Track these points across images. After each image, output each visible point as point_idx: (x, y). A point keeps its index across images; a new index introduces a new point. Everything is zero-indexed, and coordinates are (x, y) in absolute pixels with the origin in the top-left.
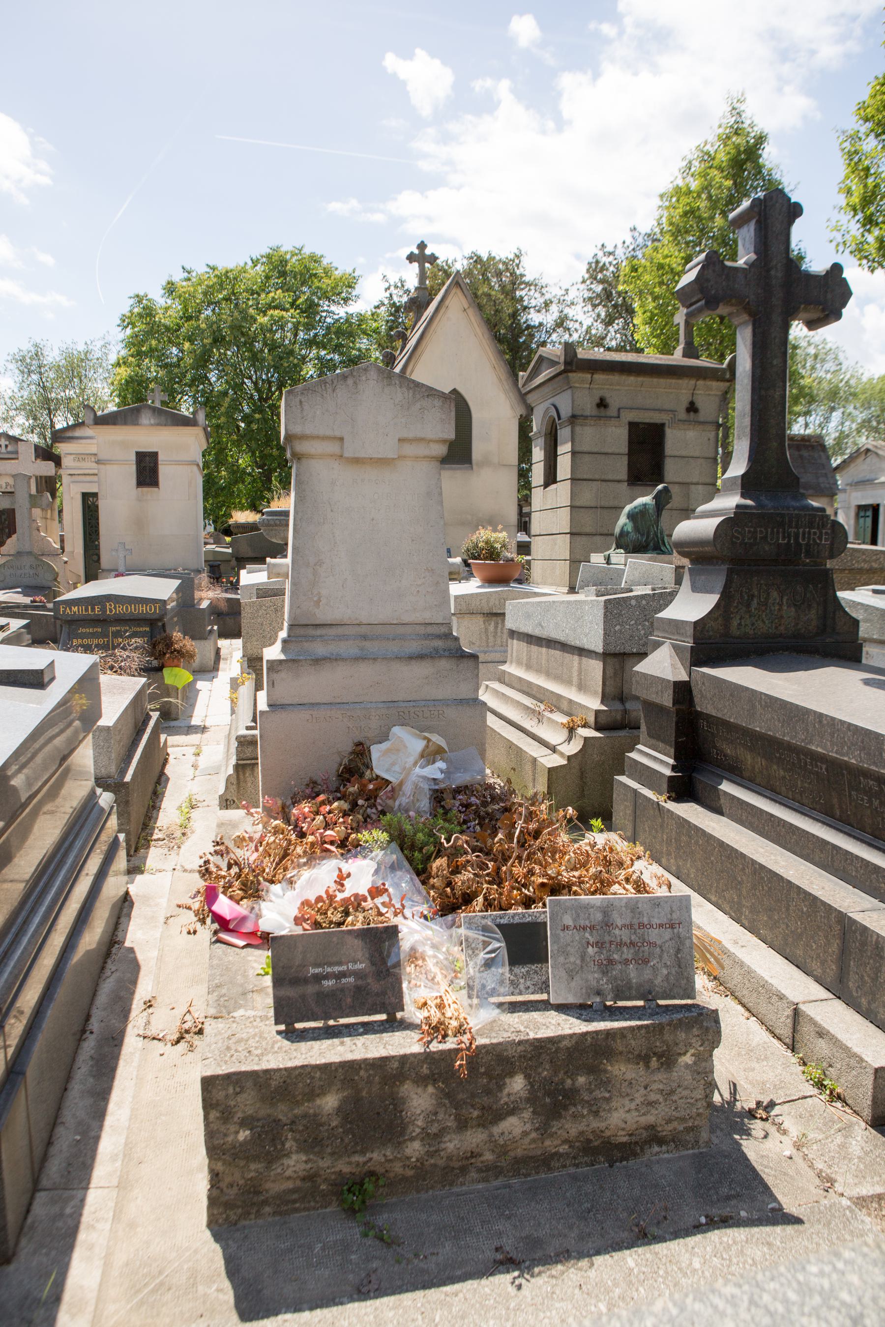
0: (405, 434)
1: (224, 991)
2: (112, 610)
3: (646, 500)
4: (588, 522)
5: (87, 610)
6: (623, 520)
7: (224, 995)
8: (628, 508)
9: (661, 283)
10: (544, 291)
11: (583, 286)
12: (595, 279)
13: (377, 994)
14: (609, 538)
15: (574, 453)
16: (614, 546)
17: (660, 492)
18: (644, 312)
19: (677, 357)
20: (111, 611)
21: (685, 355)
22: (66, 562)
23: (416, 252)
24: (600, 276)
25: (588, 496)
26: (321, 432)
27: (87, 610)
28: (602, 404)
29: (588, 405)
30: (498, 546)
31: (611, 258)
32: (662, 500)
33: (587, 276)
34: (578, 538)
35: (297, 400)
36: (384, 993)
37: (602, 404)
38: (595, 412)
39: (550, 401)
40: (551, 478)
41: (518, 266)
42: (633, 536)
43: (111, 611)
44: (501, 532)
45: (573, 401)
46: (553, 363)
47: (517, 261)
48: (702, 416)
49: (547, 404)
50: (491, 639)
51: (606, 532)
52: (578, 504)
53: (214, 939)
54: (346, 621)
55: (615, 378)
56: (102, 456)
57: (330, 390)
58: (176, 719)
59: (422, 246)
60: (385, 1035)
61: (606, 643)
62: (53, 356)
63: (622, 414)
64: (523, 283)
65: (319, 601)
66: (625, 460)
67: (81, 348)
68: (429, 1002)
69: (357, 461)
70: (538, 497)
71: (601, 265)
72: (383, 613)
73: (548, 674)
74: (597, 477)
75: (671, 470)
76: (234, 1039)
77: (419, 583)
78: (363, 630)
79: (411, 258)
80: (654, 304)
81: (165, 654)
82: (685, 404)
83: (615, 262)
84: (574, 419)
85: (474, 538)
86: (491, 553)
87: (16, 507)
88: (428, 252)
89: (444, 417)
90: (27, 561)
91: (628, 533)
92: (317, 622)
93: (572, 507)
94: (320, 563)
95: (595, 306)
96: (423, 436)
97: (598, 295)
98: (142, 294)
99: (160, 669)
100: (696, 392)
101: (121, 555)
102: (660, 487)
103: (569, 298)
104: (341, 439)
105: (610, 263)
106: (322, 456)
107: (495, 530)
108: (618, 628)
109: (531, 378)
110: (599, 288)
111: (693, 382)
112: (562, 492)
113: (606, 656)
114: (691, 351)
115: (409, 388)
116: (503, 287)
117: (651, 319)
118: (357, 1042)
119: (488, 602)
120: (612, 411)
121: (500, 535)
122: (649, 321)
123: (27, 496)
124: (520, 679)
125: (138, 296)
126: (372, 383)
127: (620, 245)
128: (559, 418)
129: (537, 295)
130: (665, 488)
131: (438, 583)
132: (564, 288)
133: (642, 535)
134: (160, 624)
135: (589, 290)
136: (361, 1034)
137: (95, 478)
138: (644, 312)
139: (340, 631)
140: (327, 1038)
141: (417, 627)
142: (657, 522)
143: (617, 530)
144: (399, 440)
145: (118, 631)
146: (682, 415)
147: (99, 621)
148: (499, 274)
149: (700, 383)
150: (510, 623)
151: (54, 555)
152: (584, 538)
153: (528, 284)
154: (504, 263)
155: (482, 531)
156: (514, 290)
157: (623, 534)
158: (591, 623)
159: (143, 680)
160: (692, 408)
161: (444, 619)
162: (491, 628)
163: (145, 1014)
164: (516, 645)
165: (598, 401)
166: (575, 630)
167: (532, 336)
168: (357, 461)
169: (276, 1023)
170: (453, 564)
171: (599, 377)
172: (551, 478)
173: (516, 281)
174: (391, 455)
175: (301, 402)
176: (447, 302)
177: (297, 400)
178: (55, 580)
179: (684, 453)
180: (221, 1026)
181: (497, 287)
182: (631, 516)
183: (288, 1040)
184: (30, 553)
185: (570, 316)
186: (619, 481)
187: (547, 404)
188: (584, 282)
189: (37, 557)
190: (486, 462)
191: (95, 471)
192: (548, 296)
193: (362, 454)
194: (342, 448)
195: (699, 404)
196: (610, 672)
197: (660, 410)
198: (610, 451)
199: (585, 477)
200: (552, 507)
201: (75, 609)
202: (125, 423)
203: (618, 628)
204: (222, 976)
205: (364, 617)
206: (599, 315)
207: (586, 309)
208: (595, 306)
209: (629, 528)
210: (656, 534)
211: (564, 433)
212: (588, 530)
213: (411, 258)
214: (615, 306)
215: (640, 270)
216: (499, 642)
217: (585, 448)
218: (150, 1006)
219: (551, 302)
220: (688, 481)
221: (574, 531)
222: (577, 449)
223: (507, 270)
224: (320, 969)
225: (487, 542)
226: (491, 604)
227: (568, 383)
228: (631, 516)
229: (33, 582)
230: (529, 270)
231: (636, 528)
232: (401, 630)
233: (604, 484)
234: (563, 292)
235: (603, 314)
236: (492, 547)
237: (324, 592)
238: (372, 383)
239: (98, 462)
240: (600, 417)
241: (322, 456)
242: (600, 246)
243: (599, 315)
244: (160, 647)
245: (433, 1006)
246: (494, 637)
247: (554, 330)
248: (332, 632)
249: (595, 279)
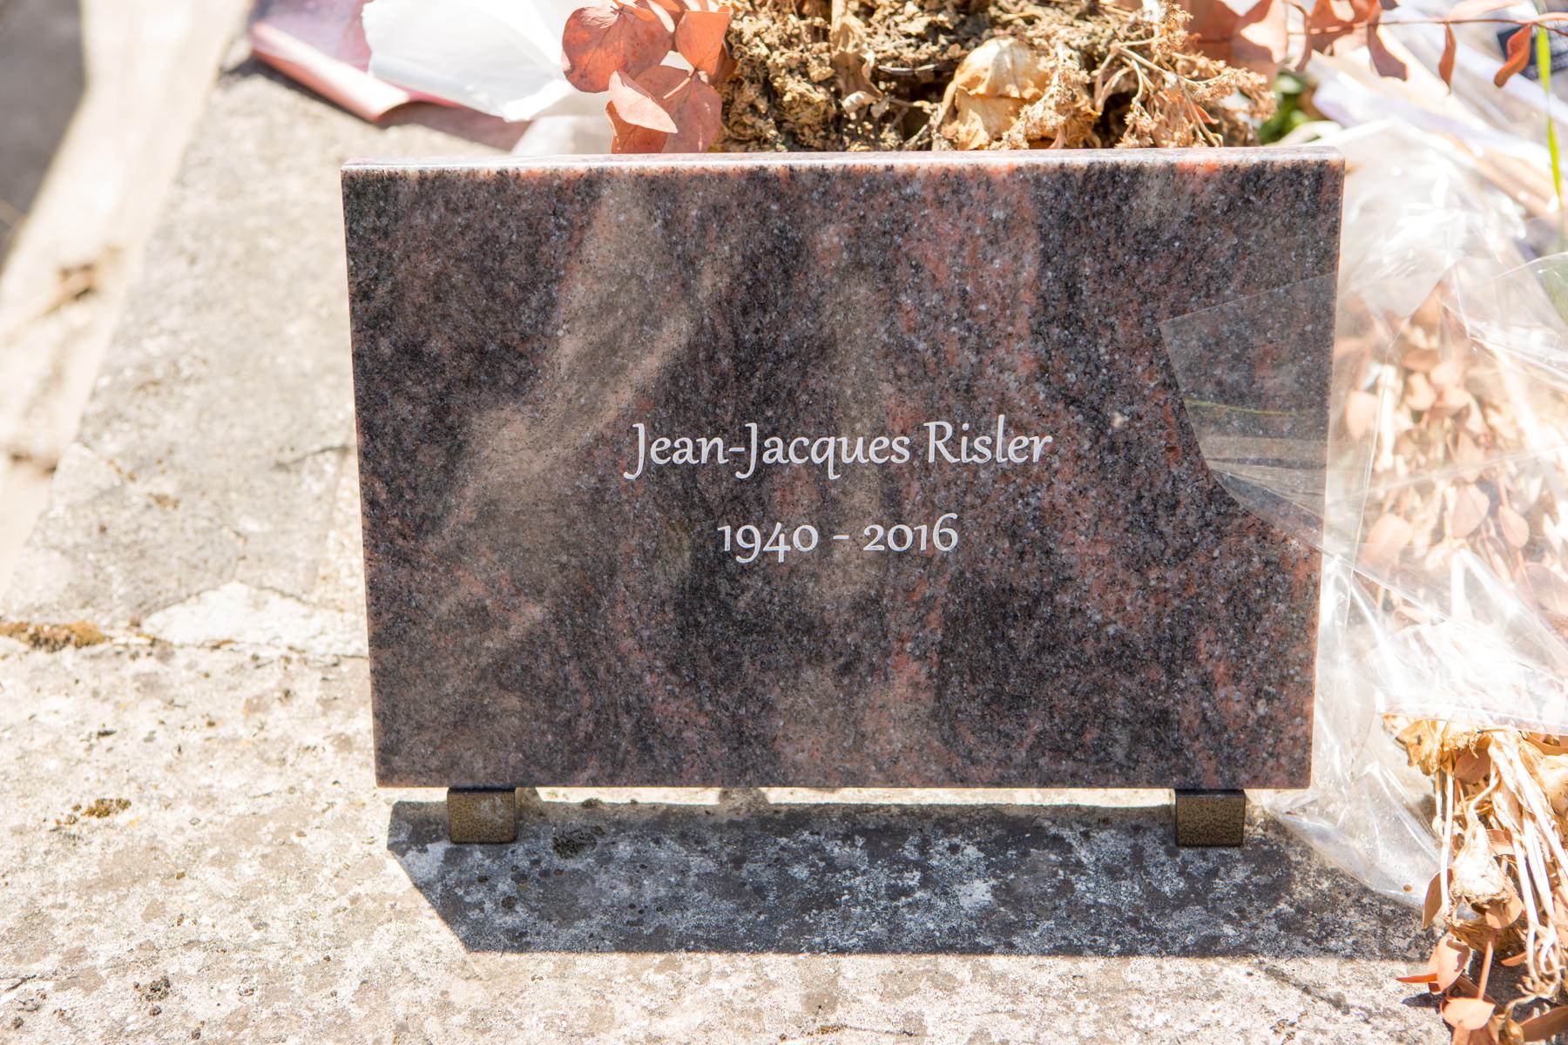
1: (173, 424)
7: (162, 460)
13: (1121, 656)
36: (1175, 649)
53: (241, 52)
60: (1143, 969)
68: (1506, 758)
76: (99, 841)
118: (931, 1008)
136: (963, 941)
140: (724, 942)
163: (53, 330)
169: (387, 774)
180: (61, 710)
183: (451, 909)
204: (200, 304)
218: (84, 293)
224: (713, 446)
245: (1536, 802)
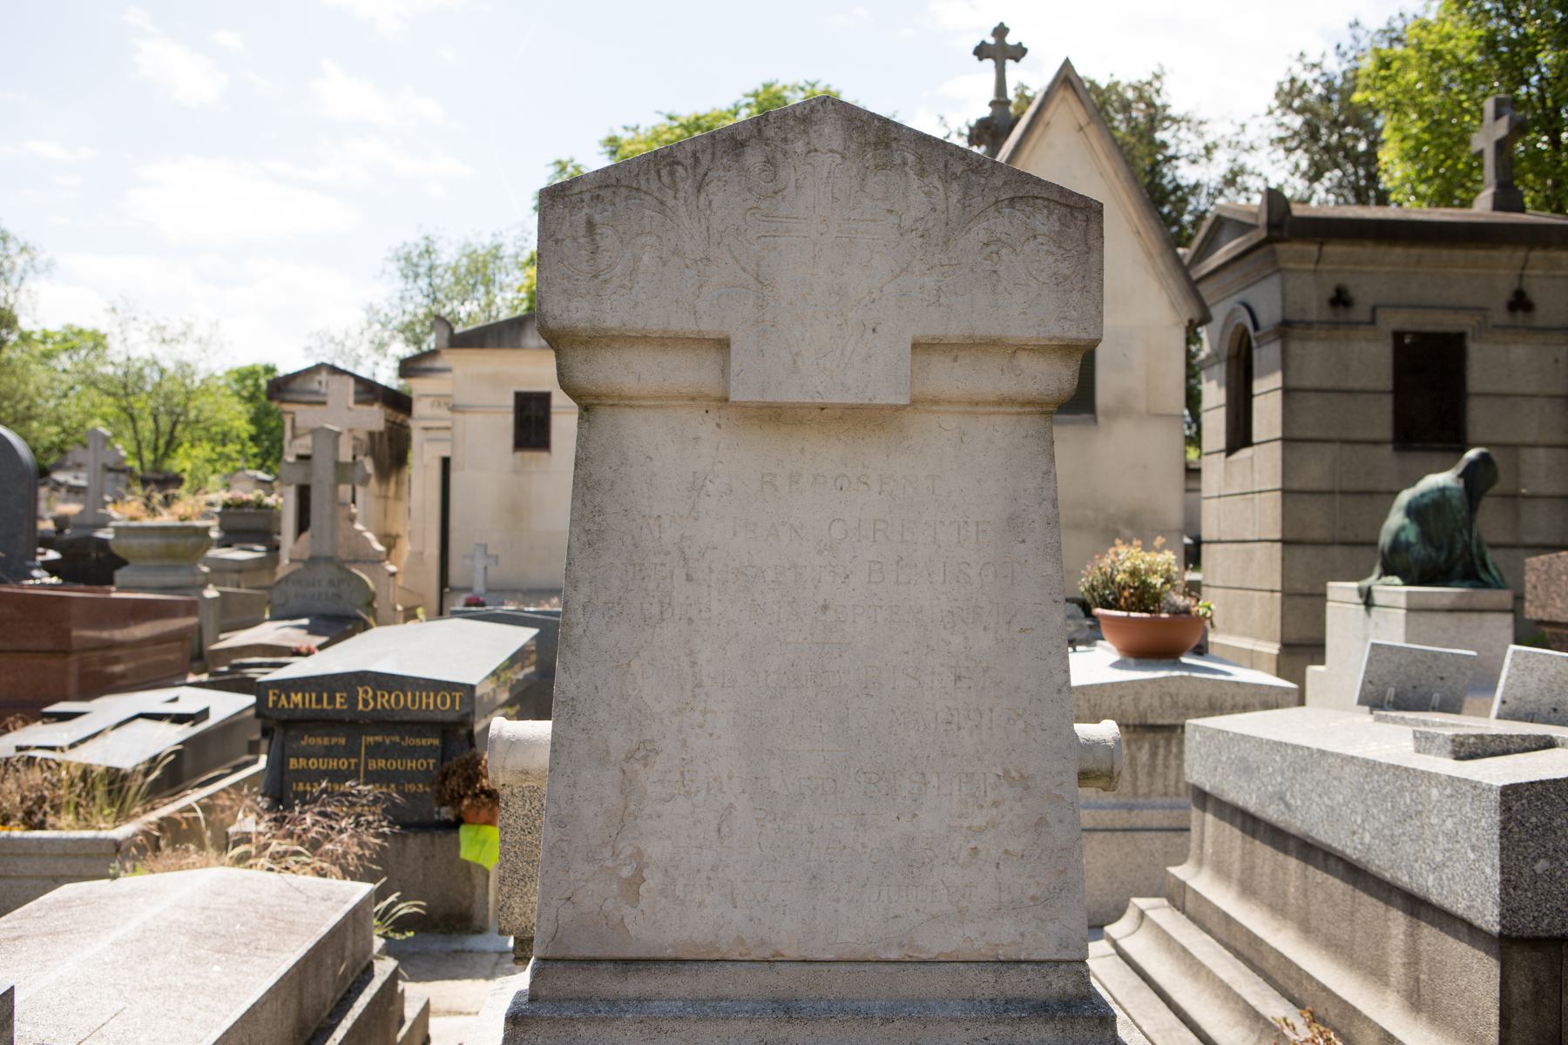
0: (934, 327)
2: (367, 700)
3: (1443, 479)
4: (1317, 521)
5: (319, 700)
6: (1396, 519)
8: (1405, 497)
9: (1434, 87)
10: (1203, 128)
11: (1270, 120)
12: (1290, 106)
14: (1367, 551)
15: (1287, 391)
16: (1378, 570)
17: (1473, 464)
18: (1403, 140)
19: (1482, 208)
20: (366, 703)
21: (1498, 205)
22: (393, 575)
23: (991, 41)
24: (1297, 103)
25: (1315, 472)
26: (655, 320)
27: (319, 700)
28: (1340, 299)
29: (1312, 301)
30: (1157, 581)
31: (1316, 73)
32: (1478, 479)
33: (1275, 103)
34: (1297, 551)
35: (580, 218)
37: (1340, 299)
38: (1327, 314)
39: (1237, 298)
40: (1239, 435)
41: (1158, 91)
42: (1420, 551)
43: (366, 703)
44: (1160, 551)
45: (1284, 296)
46: (1242, 227)
47: (1157, 84)
48: (1541, 317)
49: (1231, 303)
50: (1143, 779)
51: (1351, 538)
52: (1296, 485)
54: (725, 950)
55: (1365, 251)
56: (460, 399)
57: (686, 186)
58: (481, 931)
59: (1001, 31)
61: (1508, 909)
62: (448, 255)
63: (1382, 316)
64: (1169, 118)
65: (638, 880)
66: (1387, 403)
67: (487, 241)
69: (776, 416)
70: (1215, 470)
71: (1299, 84)
72: (855, 920)
73: (1307, 929)
74: (1333, 434)
75: (1479, 417)
77: (979, 820)
78: (783, 981)
79: (981, 52)
80: (1420, 124)
81: (462, 797)
82: (1505, 293)
83: (1323, 79)
84: (1285, 329)
85: (1106, 563)
86: (1143, 596)
87: (313, 482)
88: (1011, 40)
89: (1065, 268)
90: (325, 573)
91: (1408, 545)
92: (631, 953)
93: (1286, 492)
94: (644, 752)
95: (1289, 151)
96: (995, 331)
97: (1296, 133)
98: (565, 159)
99: (454, 825)
100: (1528, 272)
101: (479, 564)
102: (1472, 454)
103: (1245, 140)
104: (723, 344)
105: (1315, 81)
106: (662, 400)
107: (1147, 547)
108: (1541, 866)
109: (1201, 255)
110: (1296, 122)
111: (1520, 254)
112: (1263, 464)
113: (1506, 945)
114: (1507, 198)
115: (948, 177)
116: (1133, 128)
117: (1417, 149)
119: (1136, 700)
120: (1360, 312)
121: (1160, 558)
122: (1413, 155)
123: (330, 464)
124: (1227, 919)
125: (559, 162)
126: (826, 162)
127: (1331, 52)
128: (1256, 327)
129: (1191, 136)
130: (1483, 456)
131: (1041, 823)
132: (1239, 121)
133: (1439, 549)
134: (463, 732)
135: (1281, 125)
137: (447, 434)
138: (1403, 140)
139: (704, 983)
141: (971, 975)
142: (1469, 522)
143: (1385, 539)
144: (916, 346)
145: (378, 745)
146: (1500, 315)
147: (341, 722)
148: (1126, 107)
149: (1537, 255)
150: (1198, 770)
151: (375, 561)
152: (1309, 551)
153: (1175, 120)
154: (1135, 88)
155: (1123, 551)
156: (1153, 129)
157: (1397, 545)
158: (1452, 837)
159: (364, 889)
160: (1520, 302)
161: (1062, 945)
162: (1144, 756)
164: (1209, 825)
165: (1331, 293)
166: (1393, 842)
167: (1184, 200)
168: (776, 416)
170: (1092, 746)
171: (1334, 250)
172: (1239, 435)
173: (1156, 116)
174: (888, 394)
175: (591, 225)
176: (1047, 115)
177: (580, 218)
178: (370, 604)
179: (1505, 388)
181: (1123, 127)
182: (1413, 511)
184: (329, 560)
185: (1249, 167)
186: (1376, 443)
187: (1231, 303)
188: (1270, 112)
189: (341, 565)
190: (1123, 410)
191: (448, 424)
192: (1209, 139)
193: (791, 394)
194: (724, 371)
195: (1535, 293)
196: (1522, 988)
197: (1456, 309)
198: (1357, 385)
199: (1310, 434)
200: (1244, 494)
201: (297, 698)
202: (499, 345)
203: (1541, 866)
205: (788, 936)
206: (1297, 166)
207: (1274, 156)
208: (1289, 151)
209: (1411, 534)
210: (1467, 547)
211: (1265, 354)
212: (1316, 534)
213: (981, 52)
214: (1327, 149)
215: (1396, 65)
216: (1159, 785)
217: (1309, 382)
219: (1216, 146)
220: (1515, 440)
221: (1290, 536)
222: (1294, 383)
223: (1141, 98)
225: (1134, 573)
226: (1143, 705)
227: (1275, 262)
228: (1413, 511)
229: (332, 608)
230: (1175, 99)
231: (1425, 536)
232: (915, 984)
233: (1347, 448)
234: (1238, 129)
235: (1304, 165)
236: (1144, 582)
237: (655, 850)
238: (826, 162)
239: (454, 409)
240: (1335, 325)
241: (662, 400)
242: (1296, 55)
243: (1297, 166)
244: (453, 783)
246: (1150, 774)
247: (1221, 192)
248: (680, 985)
249: (1290, 106)
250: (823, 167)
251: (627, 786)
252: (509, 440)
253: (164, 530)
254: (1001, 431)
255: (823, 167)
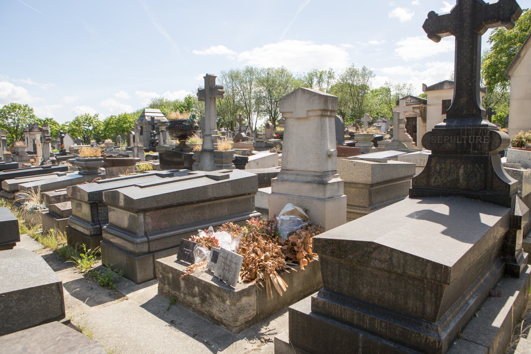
26: (288, 111)
78: (298, 172)
126: (300, 94)
174: (305, 116)
202: (438, 89)
248: (291, 172)
250: (299, 94)
251: (287, 154)
252: (441, 112)
253: (364, 135)
254: (317, 119)
255: (299, 94)
